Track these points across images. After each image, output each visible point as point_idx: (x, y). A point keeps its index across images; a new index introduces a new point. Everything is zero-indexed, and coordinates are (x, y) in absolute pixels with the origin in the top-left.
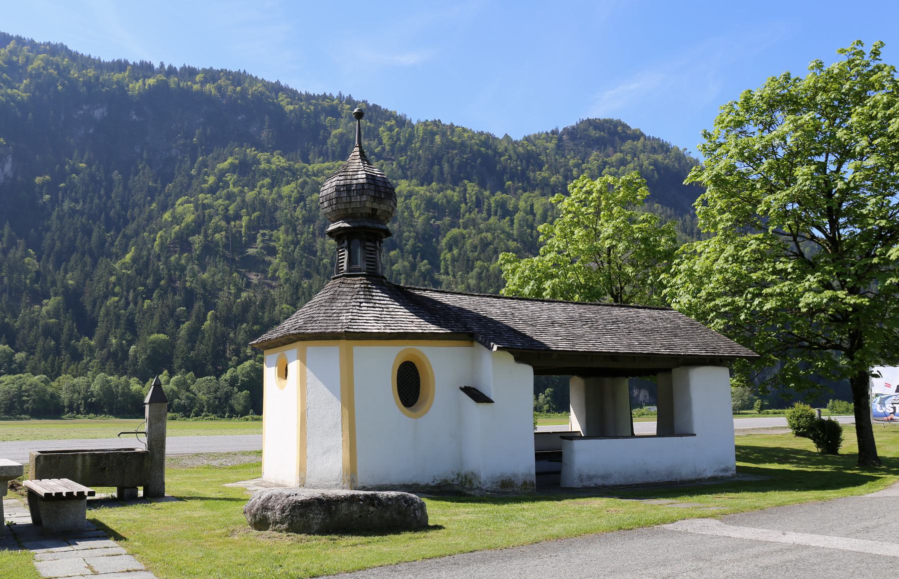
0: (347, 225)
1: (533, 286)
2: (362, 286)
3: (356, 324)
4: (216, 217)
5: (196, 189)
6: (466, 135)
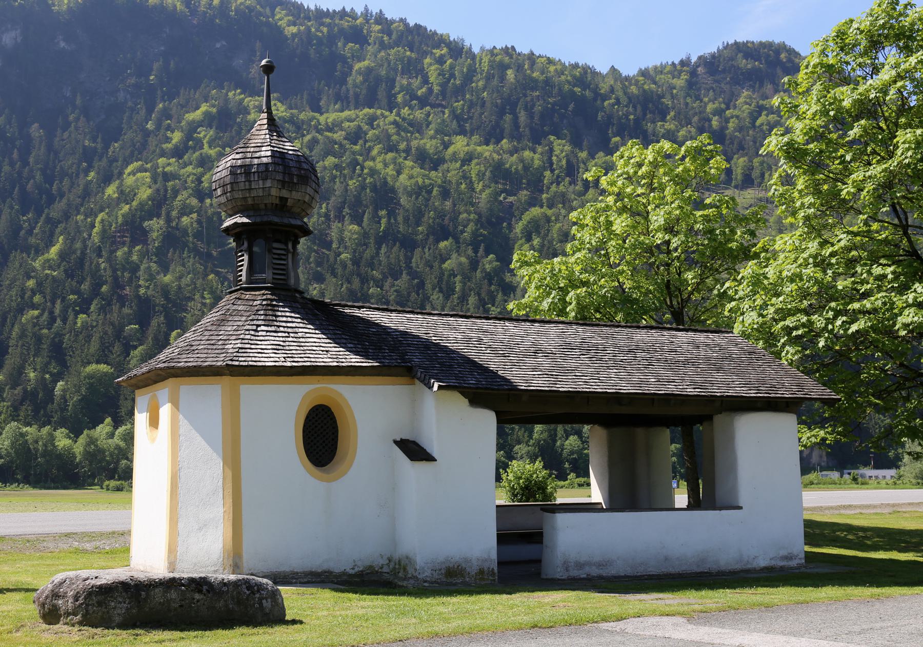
0: (245, 220)
1: (553, 298)
2: (264, 303)
3: (245, 355)
4: (184, 193)
5: (154, 151)
6: (552, 68)
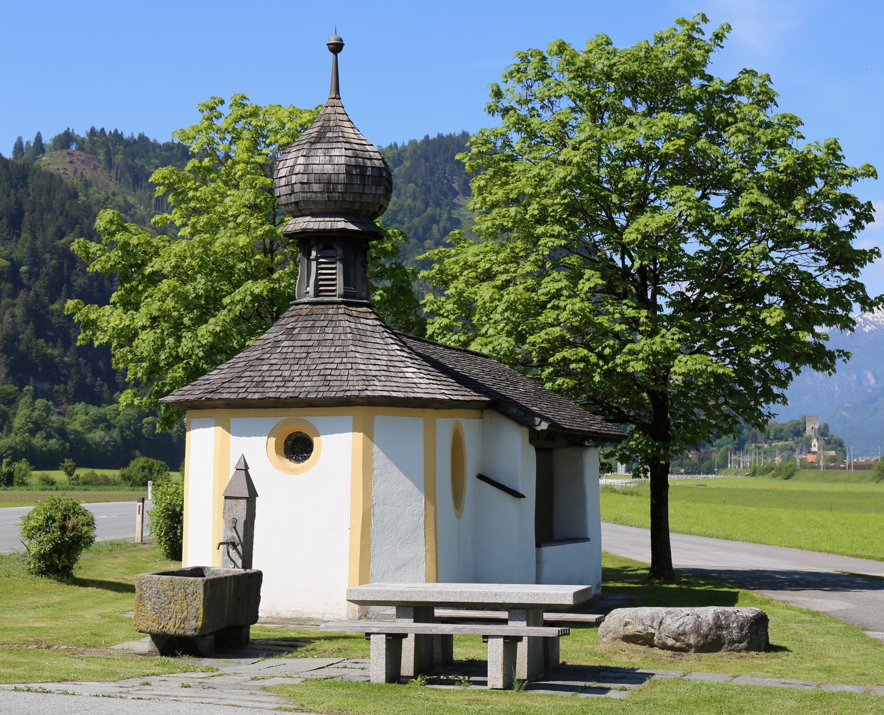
0: (351, 227)
